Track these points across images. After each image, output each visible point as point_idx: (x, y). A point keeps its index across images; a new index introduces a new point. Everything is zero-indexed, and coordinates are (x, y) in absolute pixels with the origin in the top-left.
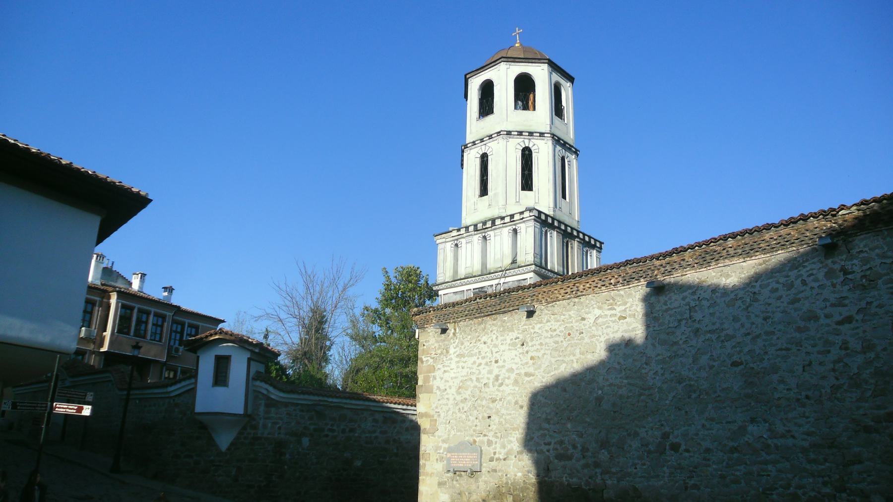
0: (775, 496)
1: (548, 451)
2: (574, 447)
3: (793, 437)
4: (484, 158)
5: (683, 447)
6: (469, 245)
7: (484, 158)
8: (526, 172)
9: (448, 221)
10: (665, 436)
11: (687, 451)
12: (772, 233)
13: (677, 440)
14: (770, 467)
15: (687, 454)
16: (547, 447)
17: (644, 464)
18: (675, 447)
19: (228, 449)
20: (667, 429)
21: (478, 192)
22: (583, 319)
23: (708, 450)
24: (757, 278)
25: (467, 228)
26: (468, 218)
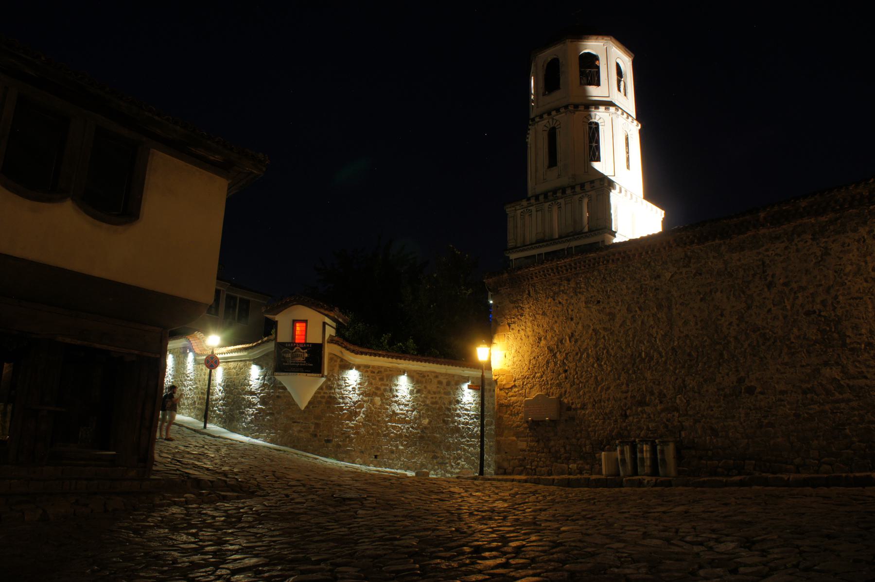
0: (847, 431)
1: (626, 398)
2: (652, 393)
3: (866, 378)
4: (552, 135)
5: (759, 390)
6: (539, 213)
7: (552, 135)
8: (594, 145)
9: (517, 189)
10: (741, 381)
11: (762, 393)
12: (486, 456)
13: (752, 384)
14: (843, 405)
15: (762, 396)
16: (624, 395)
17: (720, 407)
18: (750, 391)
19: (307, 407)
20: (742, 374)
21: (546, 163)
22: (659, 276)
23: (782, 392)
24: (264, 447)
25: (537, 197)
26: (533, 186)
